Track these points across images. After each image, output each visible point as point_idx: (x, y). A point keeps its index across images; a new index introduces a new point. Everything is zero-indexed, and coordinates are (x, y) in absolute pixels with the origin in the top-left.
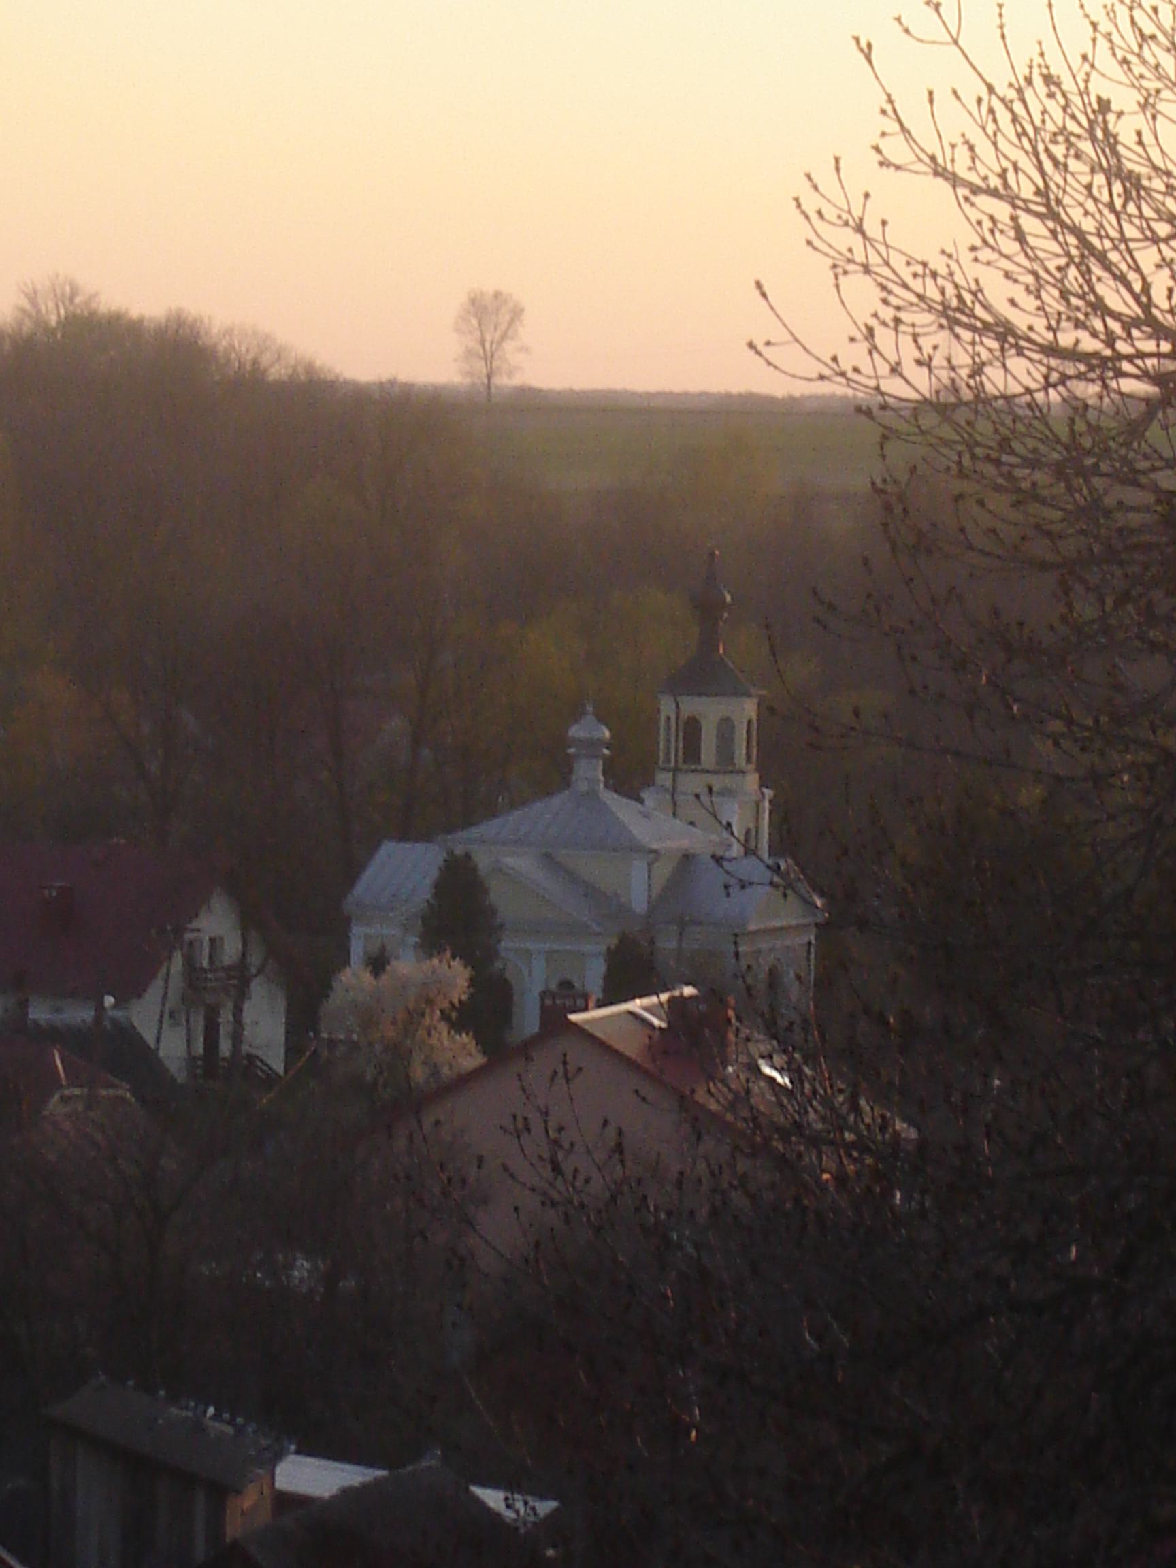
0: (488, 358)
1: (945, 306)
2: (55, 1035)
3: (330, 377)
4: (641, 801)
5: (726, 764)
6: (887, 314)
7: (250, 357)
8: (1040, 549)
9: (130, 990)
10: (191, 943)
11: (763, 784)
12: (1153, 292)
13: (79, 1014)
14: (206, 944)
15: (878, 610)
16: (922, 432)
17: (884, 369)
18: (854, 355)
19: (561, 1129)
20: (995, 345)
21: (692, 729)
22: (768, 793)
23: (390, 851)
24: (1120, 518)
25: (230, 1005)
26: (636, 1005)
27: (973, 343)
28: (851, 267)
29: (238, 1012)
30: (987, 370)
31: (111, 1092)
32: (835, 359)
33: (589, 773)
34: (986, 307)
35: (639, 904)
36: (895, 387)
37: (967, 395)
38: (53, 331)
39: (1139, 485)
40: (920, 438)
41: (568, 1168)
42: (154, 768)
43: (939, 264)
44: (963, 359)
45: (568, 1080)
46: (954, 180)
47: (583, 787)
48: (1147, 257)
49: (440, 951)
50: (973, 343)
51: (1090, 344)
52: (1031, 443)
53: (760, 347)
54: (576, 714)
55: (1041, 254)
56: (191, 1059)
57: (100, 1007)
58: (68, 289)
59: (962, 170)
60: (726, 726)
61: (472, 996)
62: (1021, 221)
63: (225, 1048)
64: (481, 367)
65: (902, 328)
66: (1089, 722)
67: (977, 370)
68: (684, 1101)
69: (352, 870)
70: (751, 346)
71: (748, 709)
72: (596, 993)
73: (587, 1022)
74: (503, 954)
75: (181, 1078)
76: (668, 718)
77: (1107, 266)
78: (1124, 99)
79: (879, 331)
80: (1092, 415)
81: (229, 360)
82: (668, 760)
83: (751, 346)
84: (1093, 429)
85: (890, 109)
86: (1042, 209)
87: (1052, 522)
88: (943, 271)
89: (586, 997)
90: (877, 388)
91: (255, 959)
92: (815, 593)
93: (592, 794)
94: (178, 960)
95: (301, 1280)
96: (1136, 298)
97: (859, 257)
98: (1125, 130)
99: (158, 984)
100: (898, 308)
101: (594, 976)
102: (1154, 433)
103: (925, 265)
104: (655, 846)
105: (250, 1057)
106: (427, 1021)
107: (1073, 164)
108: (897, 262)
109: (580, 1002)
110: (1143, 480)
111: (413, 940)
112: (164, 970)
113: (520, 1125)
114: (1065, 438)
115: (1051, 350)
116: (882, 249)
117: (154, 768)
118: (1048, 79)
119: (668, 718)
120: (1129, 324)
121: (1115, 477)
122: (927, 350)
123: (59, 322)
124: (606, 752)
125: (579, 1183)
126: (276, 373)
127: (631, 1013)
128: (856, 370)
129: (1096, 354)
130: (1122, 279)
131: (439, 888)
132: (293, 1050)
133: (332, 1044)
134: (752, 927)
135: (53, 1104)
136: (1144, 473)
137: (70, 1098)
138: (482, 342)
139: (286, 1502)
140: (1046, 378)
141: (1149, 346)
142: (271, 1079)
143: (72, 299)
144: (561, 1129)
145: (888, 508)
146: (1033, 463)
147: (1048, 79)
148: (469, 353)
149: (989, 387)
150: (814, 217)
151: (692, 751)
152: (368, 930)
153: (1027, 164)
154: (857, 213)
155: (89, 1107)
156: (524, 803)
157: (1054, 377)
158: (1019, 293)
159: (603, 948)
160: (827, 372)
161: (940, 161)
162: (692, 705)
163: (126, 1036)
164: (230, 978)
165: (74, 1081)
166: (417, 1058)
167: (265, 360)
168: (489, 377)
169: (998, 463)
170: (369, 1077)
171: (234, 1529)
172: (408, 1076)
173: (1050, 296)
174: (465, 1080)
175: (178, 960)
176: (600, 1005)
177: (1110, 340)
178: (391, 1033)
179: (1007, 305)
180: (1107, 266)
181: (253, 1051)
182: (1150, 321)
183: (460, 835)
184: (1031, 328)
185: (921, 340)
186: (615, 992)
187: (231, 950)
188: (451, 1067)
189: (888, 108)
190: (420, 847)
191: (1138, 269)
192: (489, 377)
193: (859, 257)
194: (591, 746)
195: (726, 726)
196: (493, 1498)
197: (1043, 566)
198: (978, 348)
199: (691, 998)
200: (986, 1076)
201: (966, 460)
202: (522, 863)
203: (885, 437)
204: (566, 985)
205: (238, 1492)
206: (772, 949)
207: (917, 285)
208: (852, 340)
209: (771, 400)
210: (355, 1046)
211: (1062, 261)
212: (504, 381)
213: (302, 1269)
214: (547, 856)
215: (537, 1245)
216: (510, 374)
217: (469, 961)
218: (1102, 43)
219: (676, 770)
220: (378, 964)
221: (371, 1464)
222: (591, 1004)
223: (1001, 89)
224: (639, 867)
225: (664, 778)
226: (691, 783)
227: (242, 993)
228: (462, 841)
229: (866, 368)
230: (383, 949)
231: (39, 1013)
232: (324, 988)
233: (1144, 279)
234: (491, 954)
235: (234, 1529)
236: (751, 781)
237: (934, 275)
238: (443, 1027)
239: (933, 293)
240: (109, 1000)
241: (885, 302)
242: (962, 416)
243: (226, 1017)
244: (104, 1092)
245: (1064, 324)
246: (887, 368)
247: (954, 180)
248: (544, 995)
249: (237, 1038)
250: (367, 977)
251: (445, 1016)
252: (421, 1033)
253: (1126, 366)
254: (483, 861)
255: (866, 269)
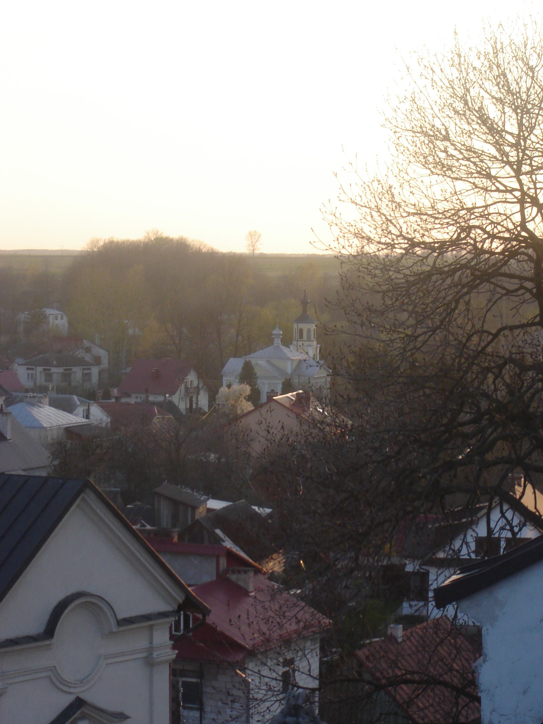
0: (253, 246)
1: (355, 234)
2: (154, 403)
3: (217, 251)
4: (289, 348)
5: (309, 339)
6: (341, 235)
7: (198, 246)
8: (377, 288)
9: (172, 393)
10: (186, 382)
11: (318, 344)
12: (403, 229)
13: (160, 399)
14: (190, 382)
15: (340, 303)
16: (350, 262)
17: (341, 247)
18: (334, 244)
19: (269, 423)
20: (366, 241)
21: (301, 331)
22: (319, 346)
23: (232, 360)
24: (396, 281)
25: (195, 396)
26: (289, 395)
27: (362, 241)
28: (332, 224)
29: (197, 398)
30: (365, 247)
31: (168, 416)
32: (329, 245)
33: (278, 342)
34: (364, 233)
35: (289, 371)
36: (344, 252)
37: (360, 253)
38: (153, 241)
39: (400, 273)
40: (350, 263)
41: (271, 432)
42: (177, 342)
43: (353, 223)
44: (359, 245)
45: (271, 411)
46: (356, 204)
47: (276, 345)
48: (401, 221)
49: (244, 383)
50: (362, 241)
51: (389, 241)
52: (376, 264)
53: (312, 242)
54: (274, 328)
55: (376, 220)
56: (187, 409)
57: (165, 397)
58: (156, 231)
59: (358, 201)
60: (309, 331)
61: (251, 393)
62: (372, 213)
63: (194, 406)
64: (252, 248)
65: (345, 238)
66: (389, 328)
67: (363, 247)
68: (298, 416)
69: (223, 366)
70: (310, 242)
71: (313, 327)
72: (280, 392)
73: (278, 399)
74: (258, 383)
75: (184, 413)
76: (296, 329)
77: (392, 223)
78: (396, 184)
79: (339, 239)
80: (390, 257)
81: (193, 248)
82: (295, 338)
83: (310, 242)
84: (390, 260)
85: (341, 188)
86: (377, 210)
87: (380, 282)
88: (354, 225)
89: (277, 393)
90: (340, 252)
91: (201, 386)
92: (325, 299)
93: (278, 347)
94: (183, 387)
95: (212, 459)
96: (399, 230)
97: (335, 222)
98: (395, 192)
99: (178, 392)
100: (344, 233)
101: (279, 388)
102: (403, 261)
103: (350, 223)
104: (293, 358)
105: (200, 408)
106: (241, 399)
107: (383, 199)
108: (344, 223)
109: (276, 395)
110: (401, 272)
111: (238, 381)
112: (180, 389)
113: (260, 422)
114: (383, 262)
115: (379, 243)
116: (340, 220)
117: (177, 342)
118: (379, 181)
119: (296, 329)
120: (397, 236)
121: (395, 271)
122: (351, 243)
123: (154, 239)
124: (281, 337)
125: (274, 435)
126: (204, 250)
127: (288, 397)
128: (335, 248)
129: (390, 243)
130: (395, 226)
131: (243, 368)
132: (210, 406)
133: (219, 405)
134: (315, 377)
135: (155, 420)
136: (401, 270)
137: (159, 418)
138: (252, 242)
139: (209, 510)
140: (378, 249)
141: (402, 241)
142: (205, 413)
143: (157, 234)
144: (269, 423)
145: (342, 279)
146: (376, 268)
147: (379, 181)
148: (249, 245)
149: (365, 251)
150: (324, 213)
151: (301, 336)
152: (227, 378)
153: (373, 200)
154: (334, 212)
155: (163, 420)
156: (263, 349)
157: (380, 249)
158: (372, 230)
159: (281, 382)
160: (328, 248)
161: (353, 199)
162: (301, 326)
163: (171, 403)
164: (195, 390)
165: (159, 414)
166: (238, 408)
167: (202, 247)
168: (254, 250)
169: (367, 268)
170: (228, 413)
171: (197, 517)
172: (236, 412)
173: (379, 230)
174: (250, 413)
175: (183, 387)
176: (280, 395)
177: (393, 240)
178: (232, 402)
179: (369, 232)
180: (392, 223)
181: (201, 407)
182: (401, 235)
183: (248, 356)
184: (374, 237)
185: (349, 241)
186: (284, 392)
187: (195, 383)
188: (246, 409)
189: (341, 187)
190: (238, 359)
191: (399, 224)
192: (254, 250)
193: (335, 222)
194: (278, 335)
195: (309, 331)
196: (256, 508)
197: (379, 292)
198: (363, 242)
199: (302, 393)
200: (366, 409)
201: (361, 268)
202: (262, 362)
203: (341, 263)
204: (273, 391)
205: (198, 508)
206: (320, 382)
207: (348, 228)
208: (334, 241)
209: (319, 255)
210: (224, 405)
211: (382, 222)
212: (257, 252)
213: (213, 456)
214: (268, 361)
215: (265, 449)
216: (258, 249)
217: (250, 385)
218: (390, 172)
219: (298, 341)
220: (229, 386)
221: (229, 501)
222: (278, 394)
223: (367, 183)
224: (289, 363)
225: (295, 343)
226: (300, 343)
227: (198, 394)
228: (248, 358)
229: (337, 247)
230: (230, 383)
231: (151, 398)
232: (217, 392)
233: (400, 226)
234: (255, 384)
235: (197, 517)
236: (315, 343)
237: (352, 226)
238: (244, 400)
239: (352, 230)
240: (167, 395)
241: (341, 232)
242: (359, 258)
243: (194, 399)
244: (166, 416)
245: (383, 237)
246: (342, 247)
247: (356, 204)
248: (267, 393)
249: (197, 403)
250: (227, 389)
251: (245, 398)
252: (239, 402)
253: (396, 246)
254: (253, 362)
255: (336, 225)
